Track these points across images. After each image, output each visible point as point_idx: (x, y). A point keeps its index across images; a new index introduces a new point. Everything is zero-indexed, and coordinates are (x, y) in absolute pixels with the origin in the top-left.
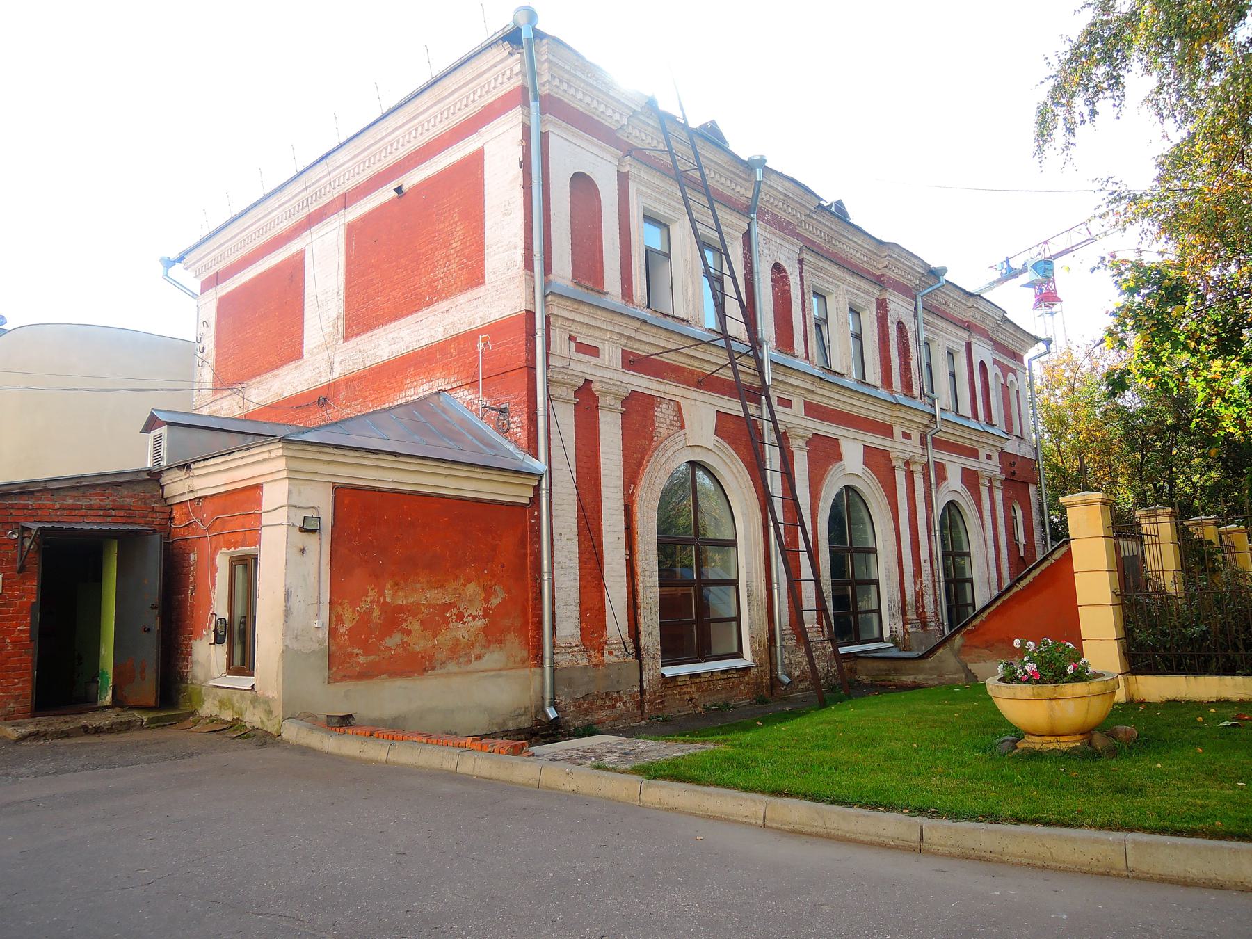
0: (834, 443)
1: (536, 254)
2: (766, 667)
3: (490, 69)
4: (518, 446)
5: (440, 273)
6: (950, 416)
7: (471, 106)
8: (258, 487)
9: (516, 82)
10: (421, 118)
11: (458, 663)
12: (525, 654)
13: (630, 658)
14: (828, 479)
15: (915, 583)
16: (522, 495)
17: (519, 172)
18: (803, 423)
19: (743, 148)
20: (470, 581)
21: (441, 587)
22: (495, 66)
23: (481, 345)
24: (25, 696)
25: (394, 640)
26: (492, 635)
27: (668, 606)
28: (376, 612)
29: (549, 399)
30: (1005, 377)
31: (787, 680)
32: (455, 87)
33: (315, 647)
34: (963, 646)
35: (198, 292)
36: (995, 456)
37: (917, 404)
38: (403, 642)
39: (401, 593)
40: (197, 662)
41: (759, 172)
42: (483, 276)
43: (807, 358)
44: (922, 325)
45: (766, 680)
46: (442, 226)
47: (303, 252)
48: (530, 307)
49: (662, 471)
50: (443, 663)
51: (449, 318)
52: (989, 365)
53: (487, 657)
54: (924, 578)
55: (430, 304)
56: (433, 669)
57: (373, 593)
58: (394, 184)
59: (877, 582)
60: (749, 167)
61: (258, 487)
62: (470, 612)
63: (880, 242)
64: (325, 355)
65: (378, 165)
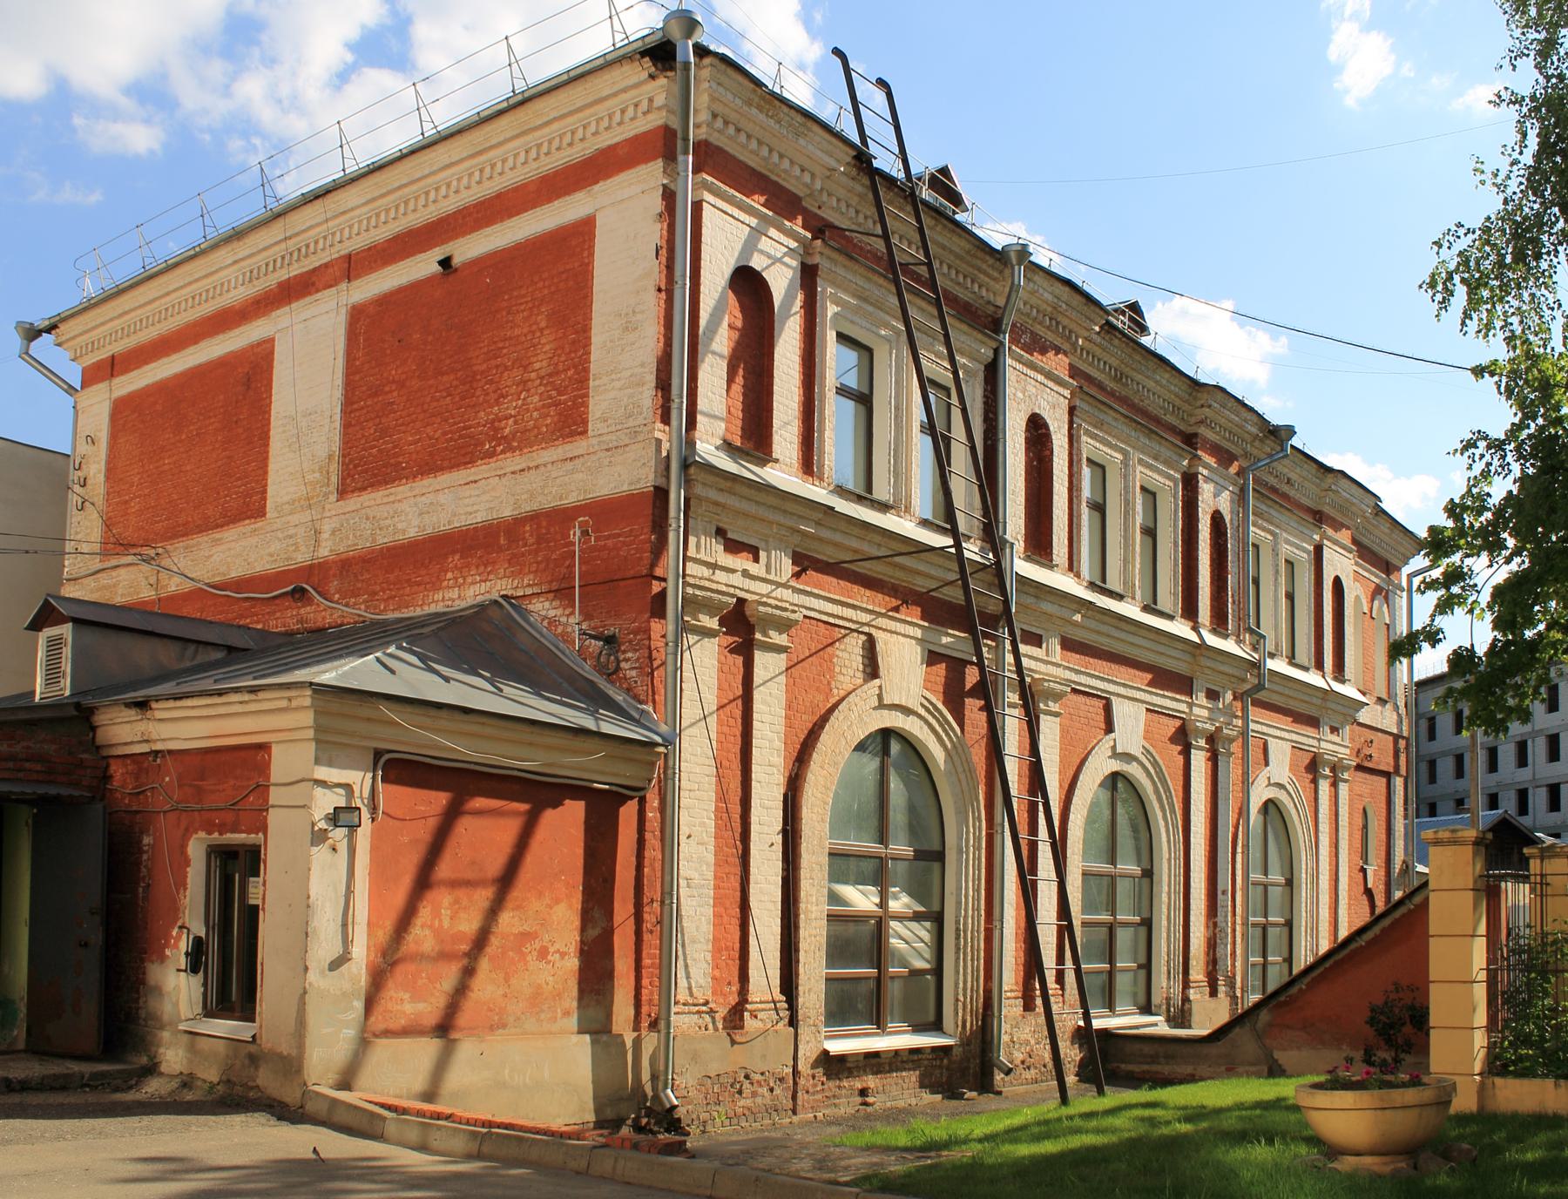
3: (615, 94)
5: (510, 407)
7: (578, 147)
8: (264, 747)
10: (491, 154)
20: (557, 901)
22: (624, 90)
23: (575, 534)
32: (555, 114)
37: (1229, 646)
39: (463, 915)
42: (585, 422)
46: (517, 332)
47: (271, 341)
48: (661, 482)
51: (533, 480)
55: (491, 454)
56: (504, 1026)
58: (438, 253)
61: (264, 747)
62: (557, 946)
63: (1195, 384)
64: (306, 516)
65: (411, 217)
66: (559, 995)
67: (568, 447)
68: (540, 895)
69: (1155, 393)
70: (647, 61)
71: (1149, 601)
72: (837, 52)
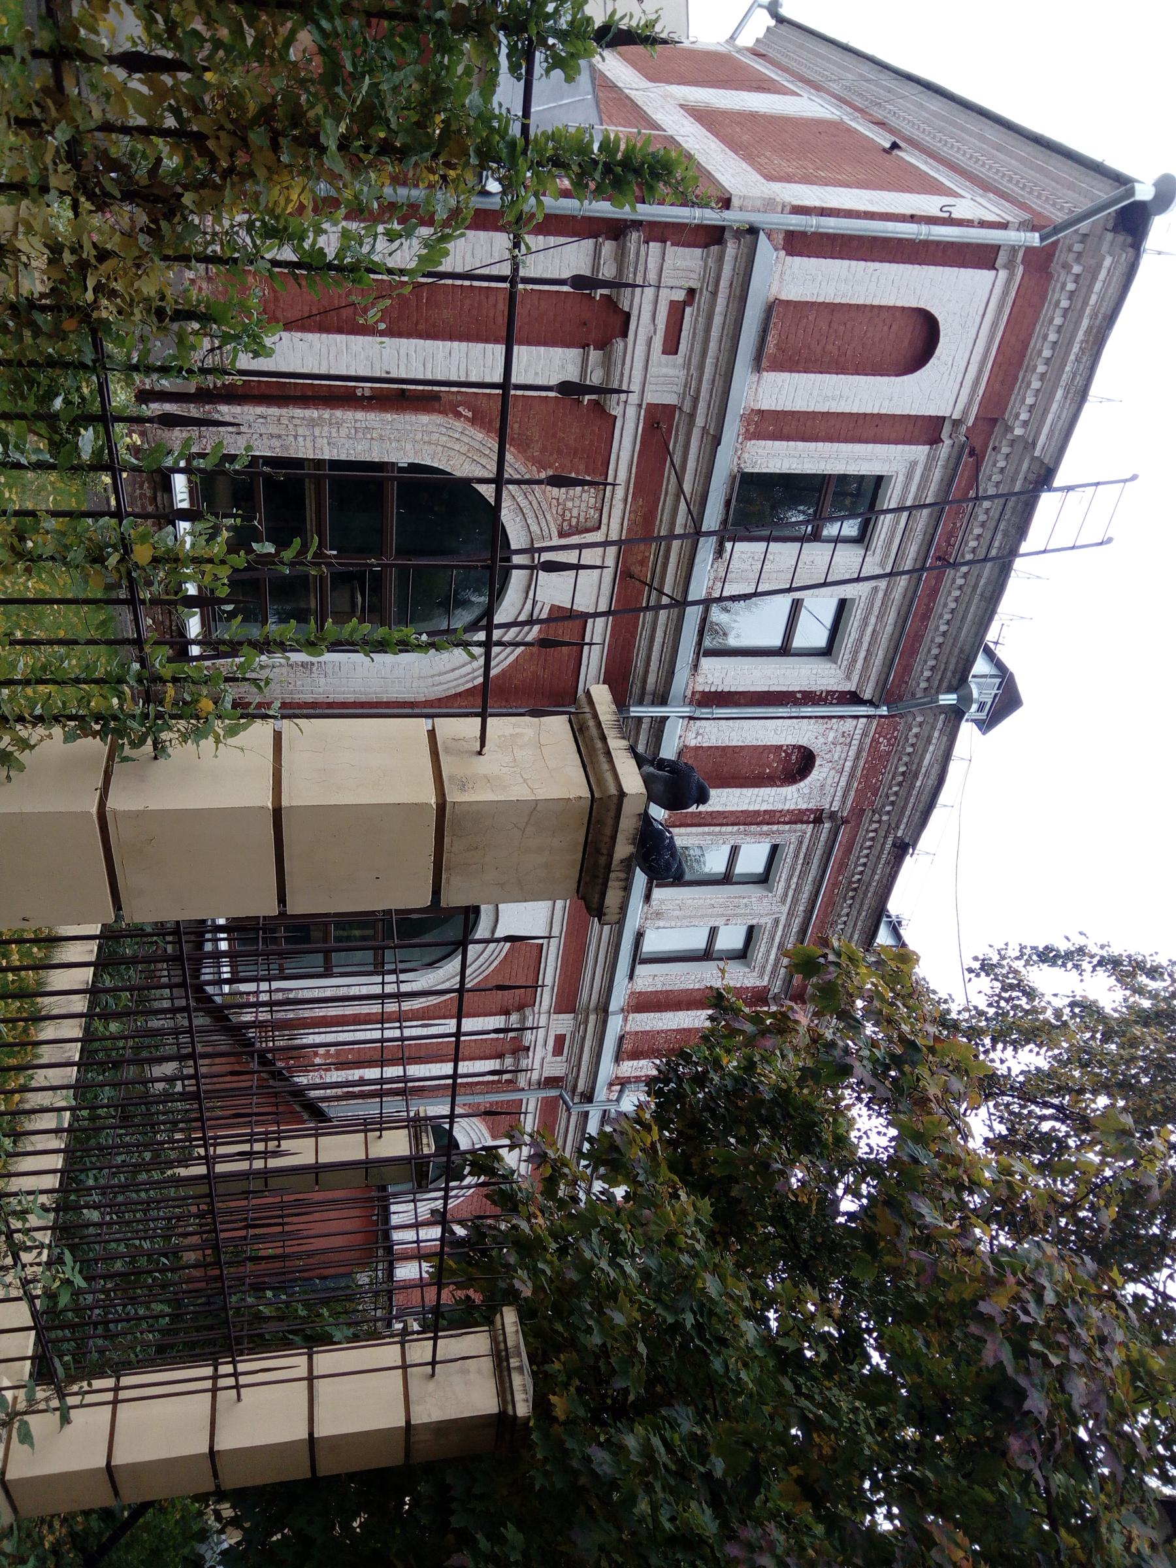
37: (607, 1068)
47: (664, 719)
72: (1134, 478)
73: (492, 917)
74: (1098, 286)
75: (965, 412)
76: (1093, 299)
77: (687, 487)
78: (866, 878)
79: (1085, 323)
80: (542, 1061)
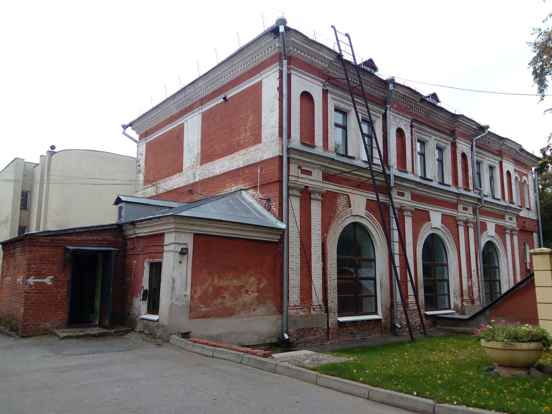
0: (427, 212)
1: (284, 130)
2: (389, 320)
4: (275, 216)
6: (489, 199)
9: (277, 51)
11: (245, 312)
12: (275, 309)
13: (323, 313)
14: (422, 230)
15: (468, 281)
16: (275, 238)
17: (277, 93)
18: (411, 204)
19: (383, 74)
20: (251, 276)
21: (239, 278)
24: (64, 319)
25: (218, 301)
26: (261, 300)
27: (341, 288)
28: (211, 289)
29: (288, 195)
30: (521, 178)
31: (399, 326)
33: (184, 303)
34: (490, 315)
35: (138, 140)
36: (514, 219)
37: (471, 194)
38: (222, 302)
39: (222, 281)
40: (135, 307)
41: (391, 87)
42: (261, 139)
43: (413, 172)
44: (475, 154)
45: (389, 326)
47: (183, 124)
48: (280, 154)
49: (340, 227)
50: (239, 312)
51: (248, 157)
52: (512, 172)
53: (257, 310)
54: (473, 279)
55: (238, 150)
56: (234, 314)
57: (209, 281)
59: (448, 281)
60: (385, 83)
61: (163, 234)
62: (251, 289)
63: (454, 116)
64: (192, 171)
66: (252, 304)
67: (257, 146)
68: (246, 274)
69: (441, 120)
70: (273, 34)
71: (441, 181)
72: (333, 27)
73: (435, 230)
74: (298, 42)
75: (321, 82)
76: (300, 43)
77: (348, 171)
78: (426, 111)
79: (305, 45)
80: (468, 215)
